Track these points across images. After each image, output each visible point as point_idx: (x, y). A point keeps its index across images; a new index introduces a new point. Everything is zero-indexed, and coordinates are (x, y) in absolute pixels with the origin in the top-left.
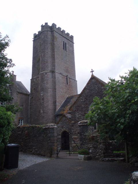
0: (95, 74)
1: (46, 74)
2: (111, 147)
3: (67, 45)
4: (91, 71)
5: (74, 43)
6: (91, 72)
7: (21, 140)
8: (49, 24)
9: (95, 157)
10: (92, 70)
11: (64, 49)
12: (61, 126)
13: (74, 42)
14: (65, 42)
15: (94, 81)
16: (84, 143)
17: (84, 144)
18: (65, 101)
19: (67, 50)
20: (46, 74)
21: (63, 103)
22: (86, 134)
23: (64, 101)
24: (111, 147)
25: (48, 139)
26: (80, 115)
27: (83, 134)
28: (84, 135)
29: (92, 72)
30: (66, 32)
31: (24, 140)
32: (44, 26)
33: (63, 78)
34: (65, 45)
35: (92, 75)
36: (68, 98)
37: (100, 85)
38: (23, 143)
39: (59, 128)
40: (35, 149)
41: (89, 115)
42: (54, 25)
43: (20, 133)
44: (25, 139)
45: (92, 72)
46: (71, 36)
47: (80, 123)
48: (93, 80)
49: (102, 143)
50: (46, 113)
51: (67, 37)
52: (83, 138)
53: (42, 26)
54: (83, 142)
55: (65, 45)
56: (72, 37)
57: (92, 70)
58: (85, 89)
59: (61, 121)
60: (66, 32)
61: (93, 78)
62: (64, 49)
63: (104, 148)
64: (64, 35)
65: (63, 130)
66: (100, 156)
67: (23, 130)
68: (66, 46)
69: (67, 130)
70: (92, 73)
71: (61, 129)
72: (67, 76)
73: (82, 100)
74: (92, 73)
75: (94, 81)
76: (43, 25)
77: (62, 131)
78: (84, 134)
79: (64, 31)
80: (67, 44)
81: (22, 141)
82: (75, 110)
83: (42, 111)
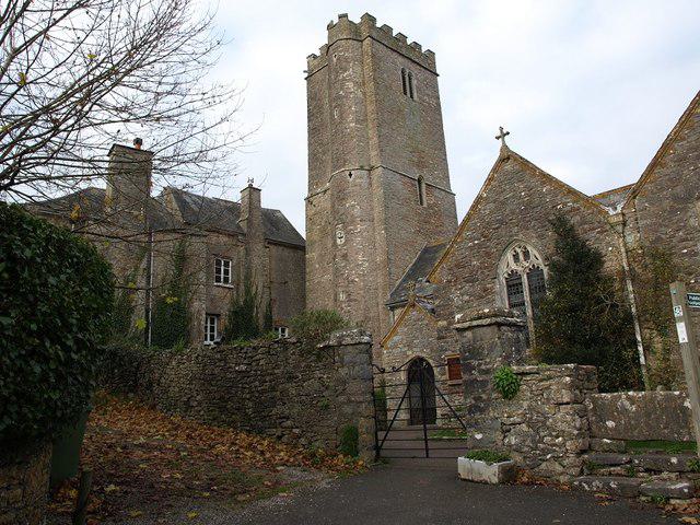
1: (350, 175)
2: (610, 424)
3: (414, 82)
4: (499, 134)
6: (498, 138)
10: (501, 129)
11: (405, 94)
13: (438, 72)
15: (511, 169)
17: (482, 411)
18: (417, 262)
19: (415, 97)
20: (350, 175)
25: (340, 388)
28: (483, 367)
29: (503, 135)
30: (409, 42)
34: (406, 80)
35: (505, 147)
36: (426, 250)
37: (534, 182)
38: (250, 405)
42: (369, 19)
43: (243, 368)
45: (503, 135)
47: (463, 320)
48: (508, 167)
49: (568, 403)
54: (478, 399)
55: (406, 80)
56: (431, 54)
57: (501, 129)
58: (479, 200)
61: (507, 156)
63: (580, 429)
64: (404, 52)
65: (411, 354)
68: (410, 82)
69: (424, 355)
72: (419, 181)
74: (503, 141)
75: (511, 169)
82: (449, 281)
83: (342, 297)
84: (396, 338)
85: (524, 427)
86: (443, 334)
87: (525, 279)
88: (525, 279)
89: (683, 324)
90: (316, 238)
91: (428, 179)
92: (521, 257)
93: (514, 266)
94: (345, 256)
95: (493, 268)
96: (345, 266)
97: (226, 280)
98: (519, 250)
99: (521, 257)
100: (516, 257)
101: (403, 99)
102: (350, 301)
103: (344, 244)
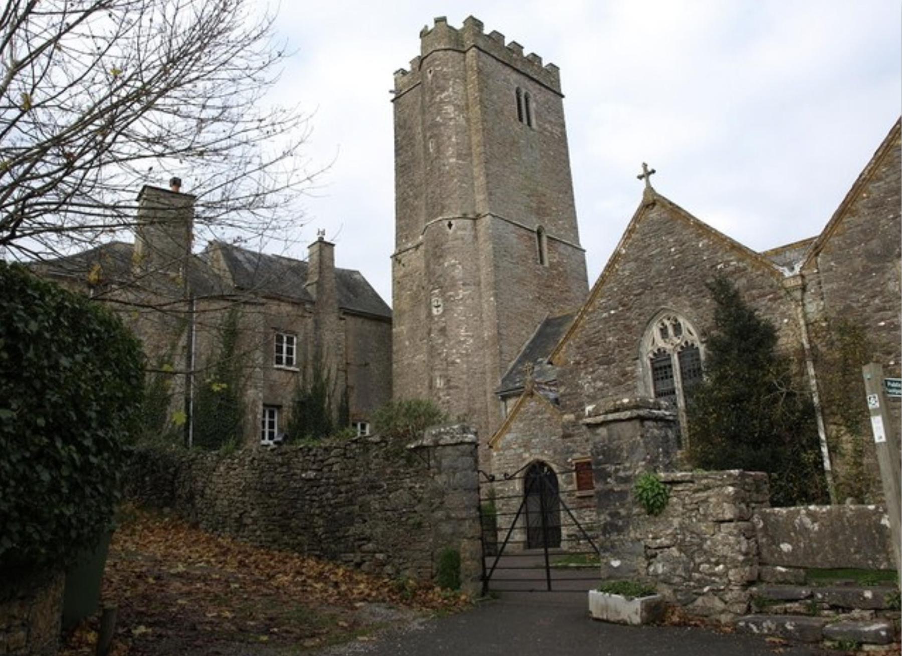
0: (663, 188)
1: (450, 225)
2: (786, 547)
3: (533, 105)
5: (563, 96)
7: (317, 512)
8: (450, 22)
9: (690, 606)
10: (645, 166)
11: (521, 119)
12: (520, 441)
13: (563, 92)
14: (523, 91)
16: (620, 523)
21: (527, 342)
22: (222, 504)
23: (532, 336)
24: (782, 546)
26: (600, 384)
27: (613, 468)
28: (621, 474)
29: (647, 173)
30: (526, 52)
31: (329, 510)
32: (431, 31)
33: (520, 236)
34: (522, 103)
35: (649, 190)
36: (548, 323)
39: (512, 452)
40: (375, 552)
41: (694, 610)
42: (474, 24)
43: (312, 474)
44: (331, 505)
45: (647, 173)
46: (551, 65)
48: (654, 214)
50: (457, 387)
51: (528, 71)
52: (612, 490)
53: (424, 34)
54: (615, 515)
55: (522, 103)
56: (553, 70)
57: (645, 166)
58: (616, 258)
59: (521, 421)
60: (526, 52)
62: (521, 119)
63: (746, 554)
64: (519, 66)
65: (529, 457)
66: (722, 600)
67: (322, 461)
70: (648, 181)
71: (520, 455)
72: (539, 233)
73: (605, 315)
74: (648, 181)
76: (430, 29)
77: (527, 462)
78: (617, 471)
79: (517, 48)
80: (531, 100)
81: (318, 515)
82: (578, 363)
83: (439, 383)
84: (509, 437)
85: (674, 551)
86: (570, 431)
87: (675, 359)
88: (675, 359)
89: (877, 440)
90: (405, 306)
91: (550, 230)
92: (671, 331)
93: (661, 343)
94: (443, 331)
95: (635, 345)
96: (443, 344)
97: (289, 362)
98: (667, 323)
99: (671, 331)
100: (664, 332)
101: (517, 127)
102: (450, 388)
103: (442, 315)
